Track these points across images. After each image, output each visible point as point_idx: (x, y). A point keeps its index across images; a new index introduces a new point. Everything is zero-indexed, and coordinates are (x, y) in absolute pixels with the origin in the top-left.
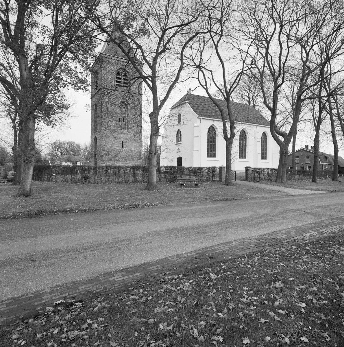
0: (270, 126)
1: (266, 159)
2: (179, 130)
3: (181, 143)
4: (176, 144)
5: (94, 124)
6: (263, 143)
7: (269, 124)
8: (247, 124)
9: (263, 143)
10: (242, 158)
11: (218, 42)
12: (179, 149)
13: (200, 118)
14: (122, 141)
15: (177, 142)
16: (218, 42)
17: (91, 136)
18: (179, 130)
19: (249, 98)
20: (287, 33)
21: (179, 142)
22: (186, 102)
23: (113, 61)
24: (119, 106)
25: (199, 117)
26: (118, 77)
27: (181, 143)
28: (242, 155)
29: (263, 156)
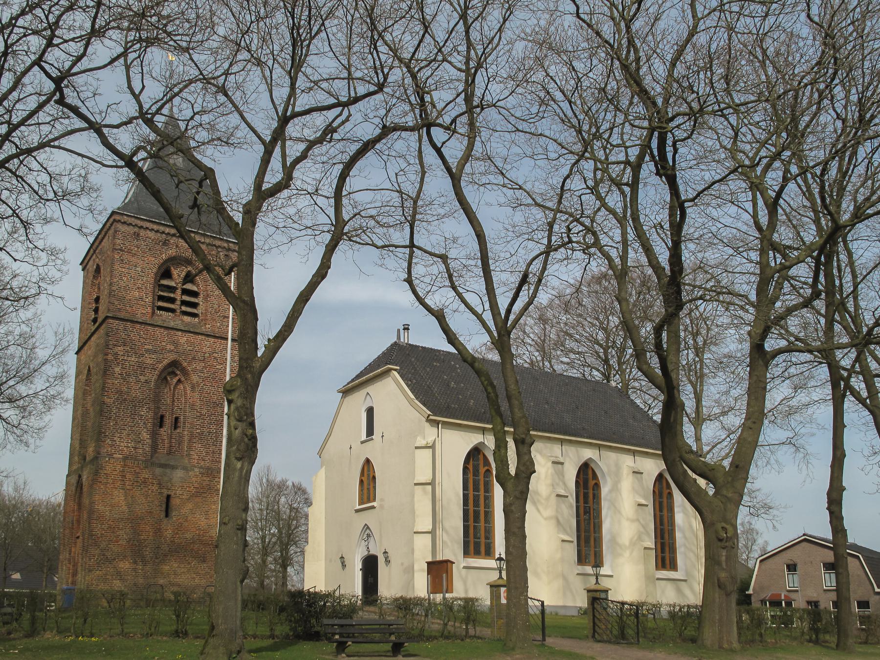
0: (663, 450)
1: (674, 567)
2: (368, 461)
3: (373, 507)
4: (357, 511)
5: (77, 436)
6: (661, 510)
7: (660, 447)
8: (562, 442)
9: (661, 510)
10: (477, 553)
11: (298, 161)
12: (366, 527)
13: (435, 421)
14: (165, 495)
15: (361, 502)
16: (298, 161)
17: (67, 476)
18: (368, 461)
19: (606, 361)
20: (625, 168)
21: (369, 501)
22: (391, 369)
23: (151, 235)
24: (163, 375)
25: (431, 417)
26: (165, 282)
27: (373, 507)
28: (477, 545)
29: (663, 560)
